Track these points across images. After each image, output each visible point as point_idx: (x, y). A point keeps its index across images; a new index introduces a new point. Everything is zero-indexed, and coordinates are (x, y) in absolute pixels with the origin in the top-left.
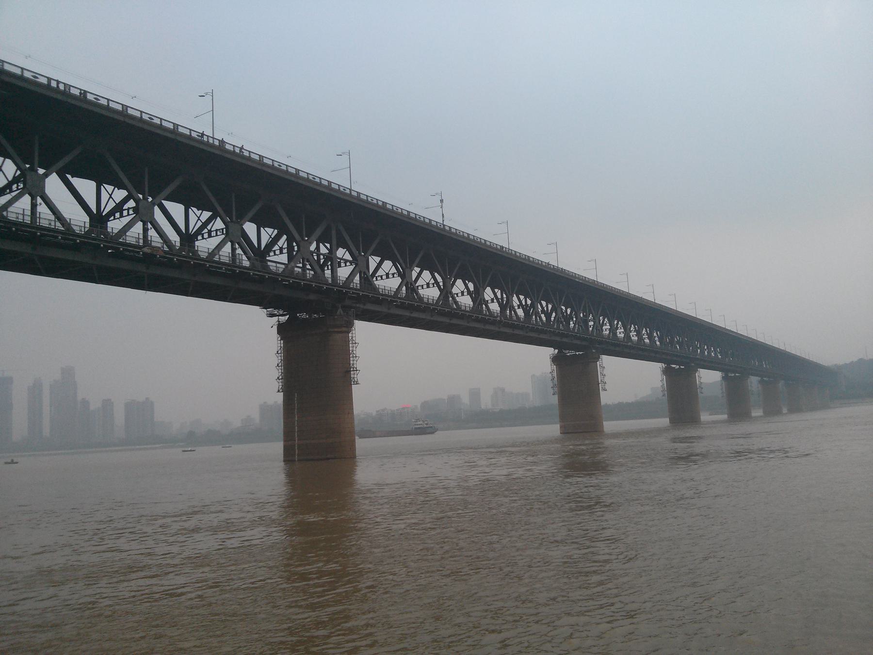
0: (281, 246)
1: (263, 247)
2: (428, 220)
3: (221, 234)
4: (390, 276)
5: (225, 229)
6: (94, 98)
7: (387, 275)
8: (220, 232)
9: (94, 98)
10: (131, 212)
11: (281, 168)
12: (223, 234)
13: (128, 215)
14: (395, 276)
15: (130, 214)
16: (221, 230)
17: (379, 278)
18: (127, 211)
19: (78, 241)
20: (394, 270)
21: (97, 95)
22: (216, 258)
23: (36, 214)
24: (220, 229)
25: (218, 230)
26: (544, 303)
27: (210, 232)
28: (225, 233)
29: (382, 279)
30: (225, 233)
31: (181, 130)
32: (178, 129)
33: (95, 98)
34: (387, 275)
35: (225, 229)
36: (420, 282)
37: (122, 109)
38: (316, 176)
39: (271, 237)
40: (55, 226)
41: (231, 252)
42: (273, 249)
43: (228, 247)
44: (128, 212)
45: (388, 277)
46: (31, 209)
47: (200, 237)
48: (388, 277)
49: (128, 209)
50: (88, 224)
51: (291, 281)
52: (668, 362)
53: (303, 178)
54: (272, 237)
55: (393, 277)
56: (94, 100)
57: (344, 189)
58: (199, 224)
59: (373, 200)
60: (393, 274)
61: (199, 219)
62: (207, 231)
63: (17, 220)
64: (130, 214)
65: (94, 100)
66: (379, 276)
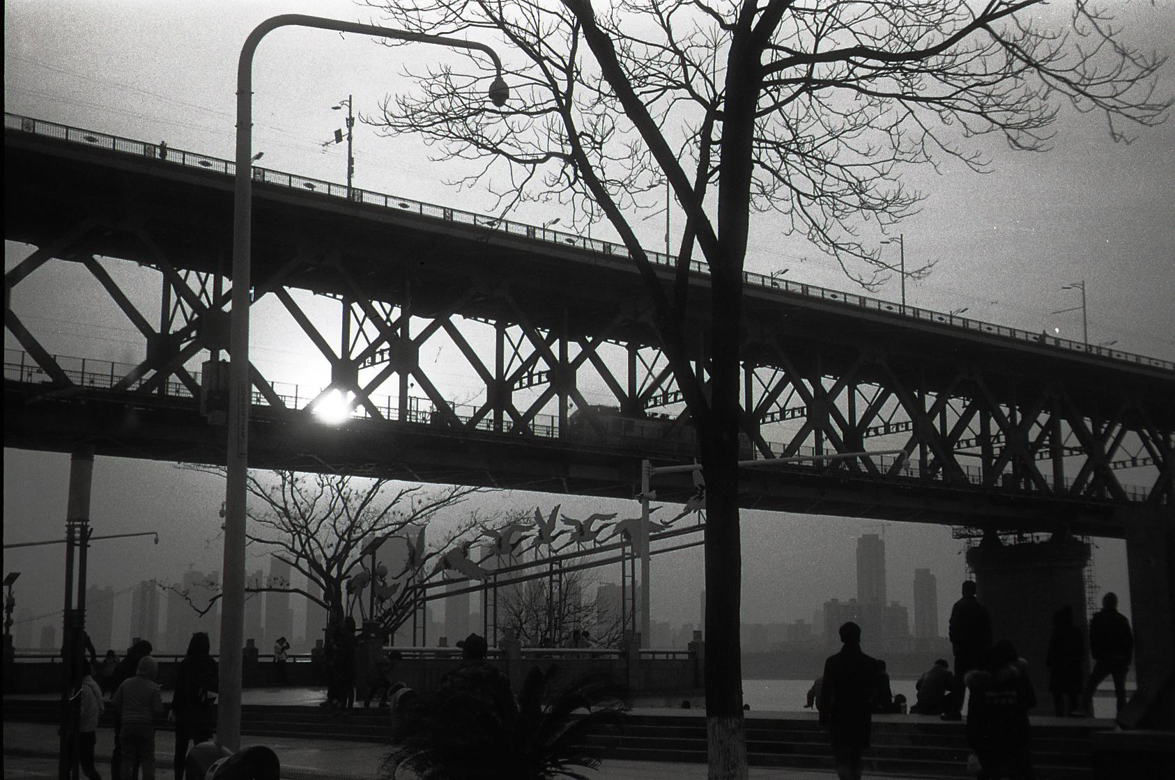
0: (782, 407)
1: (857, 422)
2: (1008, 331)
3: (800, 415)
4: (1139, 462)
5: (805, 409)
6: (305, 185)
7: (1134, 460)
8: (902, 427)
9: (305, 185)
10: (544, 378)
11: (992, 331)
12: (803, 415)
13: (540, 382)
14: (1148, 462)
15: (542, 381)
16: (904, 425)
17: (1119, 466)
18: (537, 376)
19: (83, 402)
20: (1145, 453)
21: (310, 179)
22: (903, 473)
23: (1063, 481)
24: (902, 423)
25: (796, 409)
26: (1005, 410)
27: (530, 376)
28: (805, 413)
29: (1125, 467)
30: (805, 413)
31: (457, 218)
32: (918, 314)
33: (203, 163)
34: (1134, 460)
35: (805, 409)
36: (1119, 455)
37: (444, 216)
38: (893, 304)
39: (767, 390)
40: (82, 382)
41: (981, 466)
42: (654, 395)
43: (810, 440)
44: (540, 379)
45: (1134, 464)
46: (1054, 473)
47: (517, 385)
48: (887, 431)
49: (540, 374)
50: (1052, 478)
51: (1012, 498)
52: (990, 527)
53: (872, 311)
54: (770, 389)
55: (898, 431)
56: (200, 165)
57: (888, 307)
58: (650, 381)
59: (891, 308)
60: (1145, 460)
61: (650, 373)
62: (661, 393)
63: (91, 385)
64: (542, 381)
65: (200, 165)
66: (962, 440)
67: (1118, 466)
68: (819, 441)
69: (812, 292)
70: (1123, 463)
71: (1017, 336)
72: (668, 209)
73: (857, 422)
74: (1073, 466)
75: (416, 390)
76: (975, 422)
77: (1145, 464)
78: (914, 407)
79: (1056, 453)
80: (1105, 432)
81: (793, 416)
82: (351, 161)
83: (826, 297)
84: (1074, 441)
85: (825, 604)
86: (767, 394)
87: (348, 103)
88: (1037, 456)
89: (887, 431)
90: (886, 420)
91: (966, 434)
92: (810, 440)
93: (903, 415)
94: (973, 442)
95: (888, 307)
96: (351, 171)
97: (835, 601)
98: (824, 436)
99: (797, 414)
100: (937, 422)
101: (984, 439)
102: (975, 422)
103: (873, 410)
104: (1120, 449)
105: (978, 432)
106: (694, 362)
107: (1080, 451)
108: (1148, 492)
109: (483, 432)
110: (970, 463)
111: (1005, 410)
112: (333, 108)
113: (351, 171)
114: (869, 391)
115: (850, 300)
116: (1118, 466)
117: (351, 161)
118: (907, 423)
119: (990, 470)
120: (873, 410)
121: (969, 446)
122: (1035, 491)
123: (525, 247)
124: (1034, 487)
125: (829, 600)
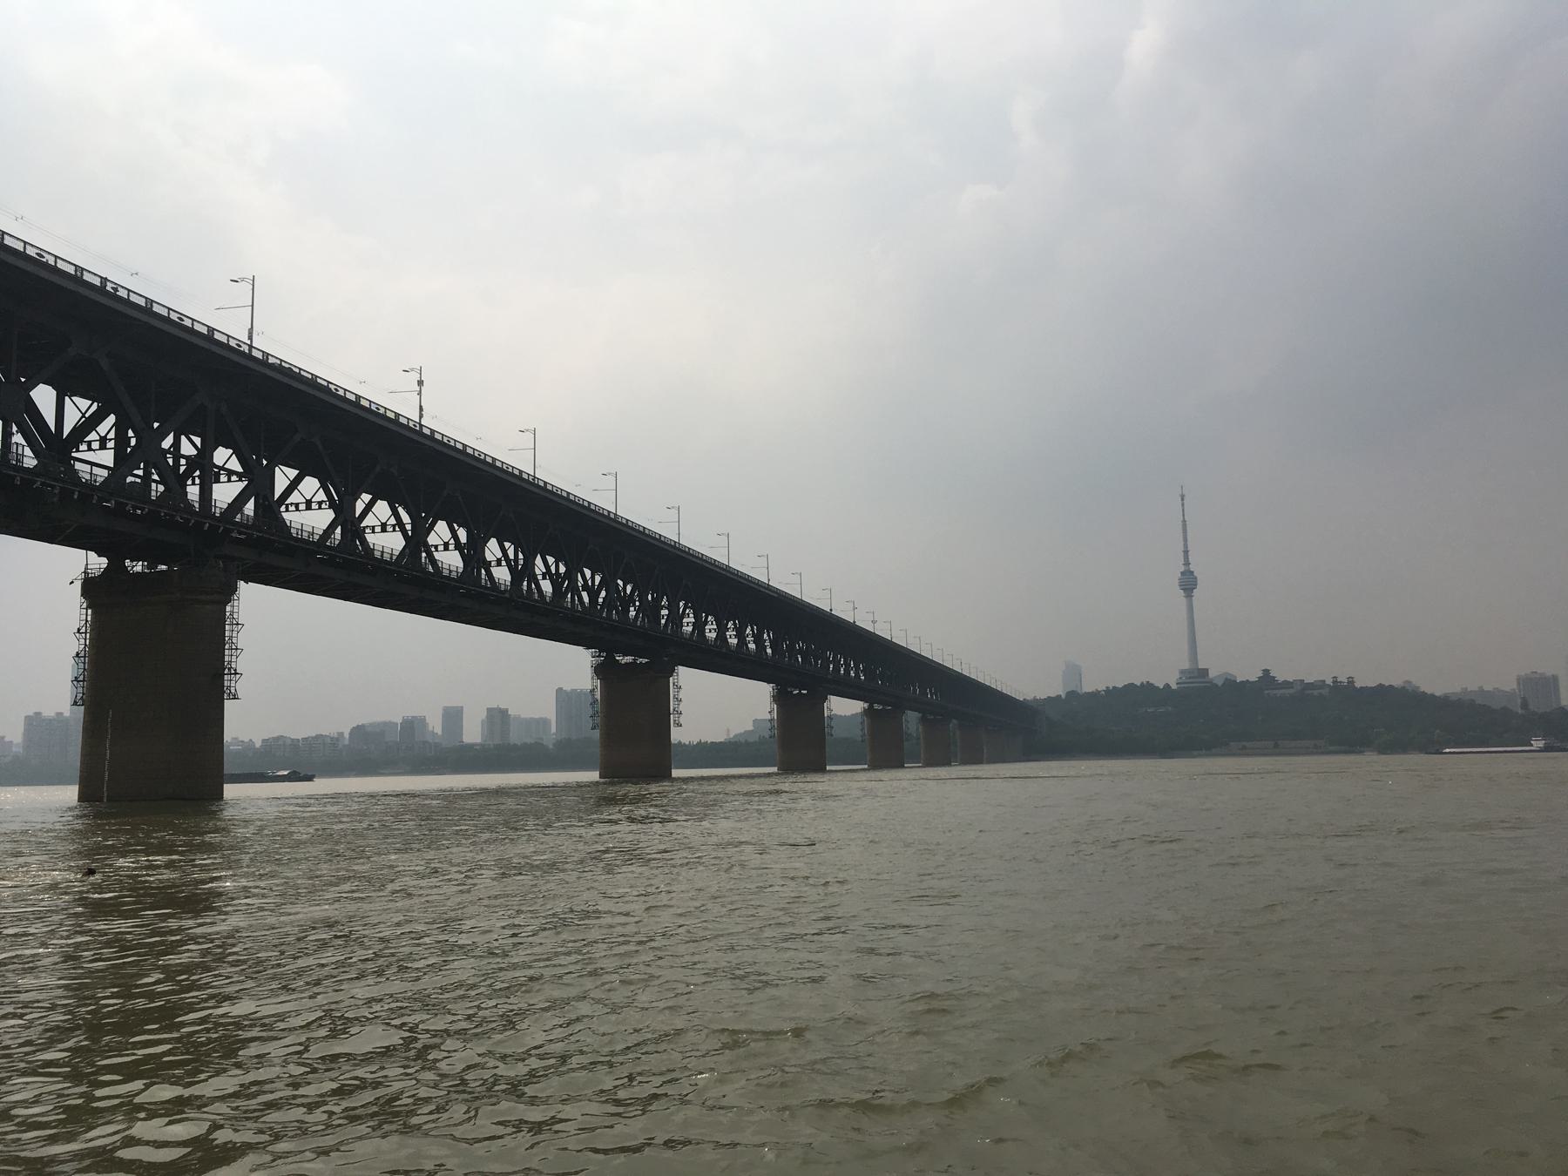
4: (314, 506)
14: (323, 506)
20: (321, 496)
26: (588, 573)
36: (369, 521)
39: (83, 416)
54: (87, 415)
57: (237, 345)
60: (320, 503)
66: (292, 504)
67: (291, 508)
69: (217, 336)
71: (270, 361)
72: (252, 306)
83: (230, 343)
85: (26, 717)
86: (84, 419)
87: (251, 282)
90: (103, 435)
95: (179, 318)
97: (38, 714)
107: (240, 476)
111: (588, 573)
112: (232, 281)
115: (197, 327)
116: (291, 508)
121: (90, 449)
123: (71, 286)
124: (614, 616)
125: (31, 714)
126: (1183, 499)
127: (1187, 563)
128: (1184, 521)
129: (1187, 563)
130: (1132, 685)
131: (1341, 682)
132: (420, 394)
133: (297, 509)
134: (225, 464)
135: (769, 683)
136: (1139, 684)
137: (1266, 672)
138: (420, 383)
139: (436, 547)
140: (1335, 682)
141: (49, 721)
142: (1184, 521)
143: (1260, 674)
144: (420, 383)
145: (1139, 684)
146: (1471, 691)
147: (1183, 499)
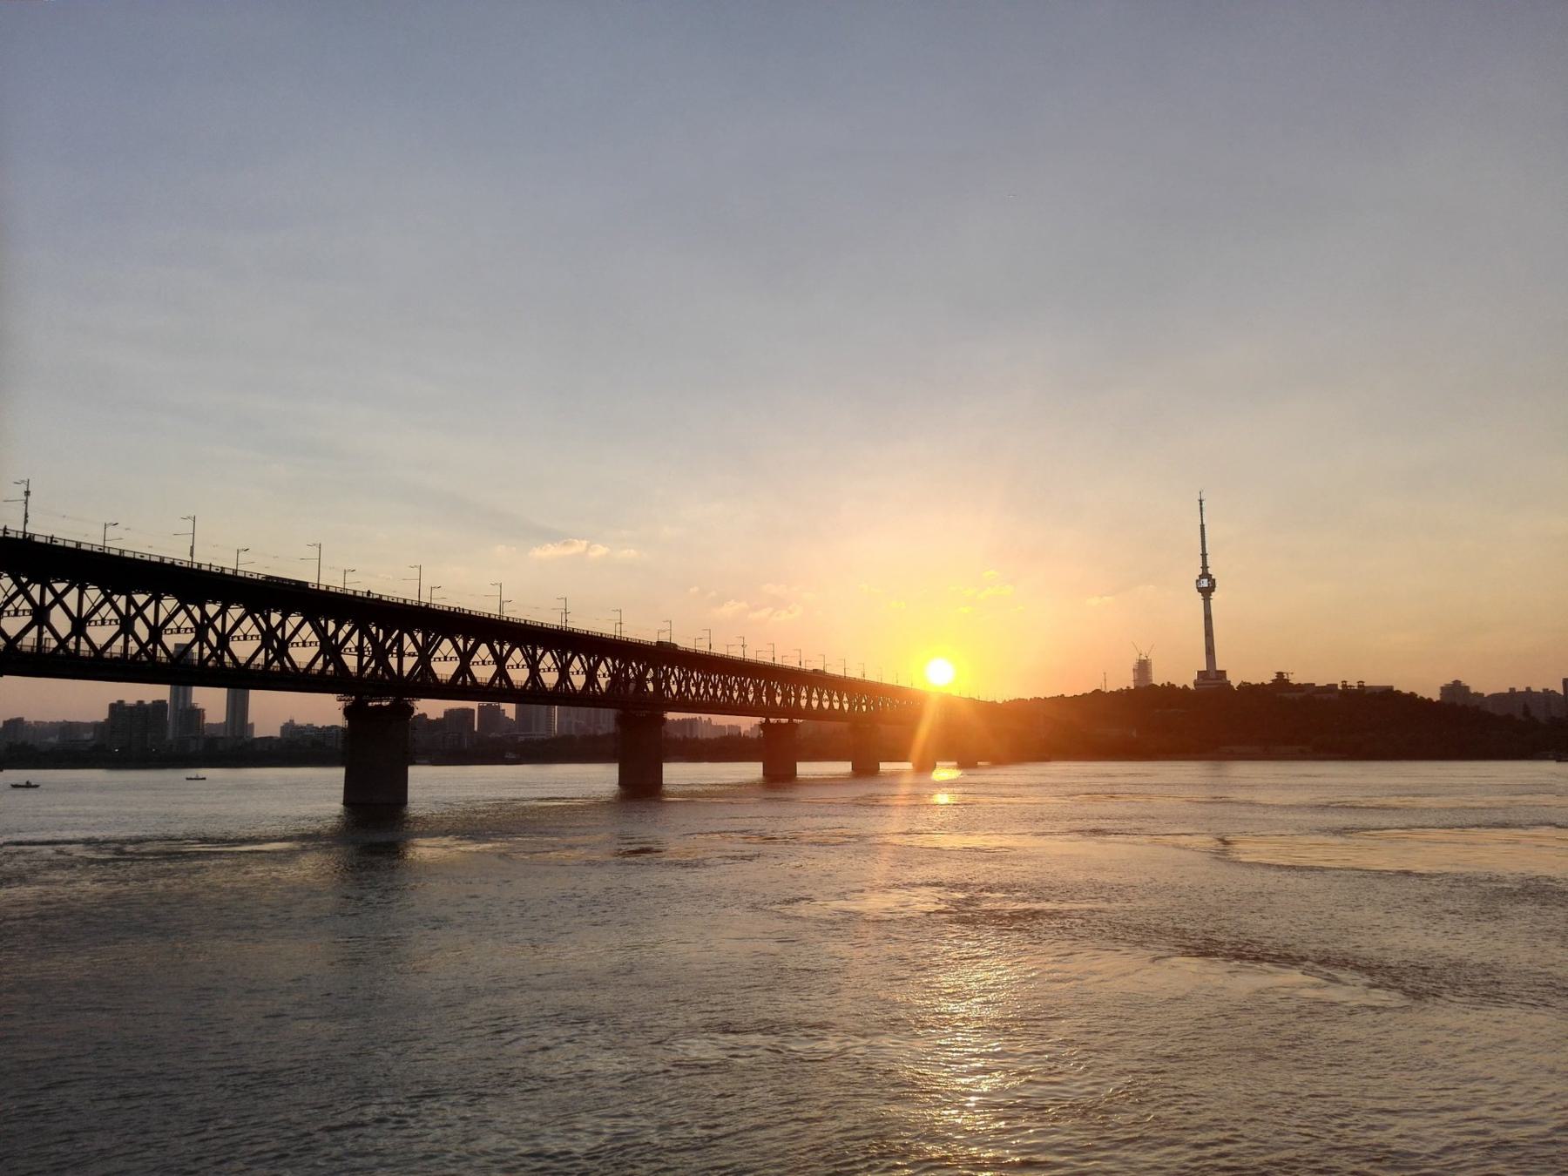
1: (227, 632)
4: (520, 667)
34: (518, 666)
39: (6, 594)
43: (120, 641)
54: (96, 604)
60: (523, 666)
68: (126, 641)
70: (512, 666)
73: (227, 632)
74: (409, 663)
75: (47, 635)
76: (355, 637)
77: (451, 660)
78: (321, 631)
79: (401, 655)
80: (255, 617)
81: (110, 624)
82: (26, 516)
84: (412, 649)
88: (432, 660)
89: (304, 645)
91: (349, 645)
92: (120, 641)
93: (314, 638)
94: (353, 650)
96: (26, 522)
98: (270, 652)
99: (254, 638)
100: (279, 633)
101: (360, 649)
102: (355, 637)
103: (171, 617)
104: (438, 651)
105: (357, 644)
106: (17, 589)
108: (449, 678)
109: (728, 712)
110: (351, 661)
113: (26, 522)
114: (169, 603)
117: (26, 516)
118: (316, 642)
119: (361, 668)
120: (171, 617)
122: (167, 663)
126: (1201, 504)
127: (1205, 567)
128: (1202, 526)
129: (1205, 567)
130: (1400, 692)
131: (1351, 686)
132: (26, 503)
133: (440, 660)
134: (3, 589)
135: (333, 693)
136: (1159, 685)
137: (1280, 674)
138: (27, 493)
139: (573, 673)
140: (1344, 686)
141: (131, 708)
142: (1202, 526)
143: (1274, 677)
144: (27, 493)
145: (1159, 685)
146: (1519, 692)
147: (1201, 504)
